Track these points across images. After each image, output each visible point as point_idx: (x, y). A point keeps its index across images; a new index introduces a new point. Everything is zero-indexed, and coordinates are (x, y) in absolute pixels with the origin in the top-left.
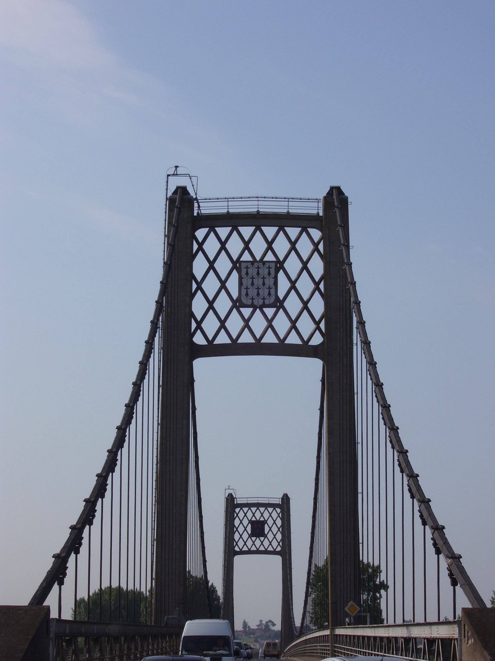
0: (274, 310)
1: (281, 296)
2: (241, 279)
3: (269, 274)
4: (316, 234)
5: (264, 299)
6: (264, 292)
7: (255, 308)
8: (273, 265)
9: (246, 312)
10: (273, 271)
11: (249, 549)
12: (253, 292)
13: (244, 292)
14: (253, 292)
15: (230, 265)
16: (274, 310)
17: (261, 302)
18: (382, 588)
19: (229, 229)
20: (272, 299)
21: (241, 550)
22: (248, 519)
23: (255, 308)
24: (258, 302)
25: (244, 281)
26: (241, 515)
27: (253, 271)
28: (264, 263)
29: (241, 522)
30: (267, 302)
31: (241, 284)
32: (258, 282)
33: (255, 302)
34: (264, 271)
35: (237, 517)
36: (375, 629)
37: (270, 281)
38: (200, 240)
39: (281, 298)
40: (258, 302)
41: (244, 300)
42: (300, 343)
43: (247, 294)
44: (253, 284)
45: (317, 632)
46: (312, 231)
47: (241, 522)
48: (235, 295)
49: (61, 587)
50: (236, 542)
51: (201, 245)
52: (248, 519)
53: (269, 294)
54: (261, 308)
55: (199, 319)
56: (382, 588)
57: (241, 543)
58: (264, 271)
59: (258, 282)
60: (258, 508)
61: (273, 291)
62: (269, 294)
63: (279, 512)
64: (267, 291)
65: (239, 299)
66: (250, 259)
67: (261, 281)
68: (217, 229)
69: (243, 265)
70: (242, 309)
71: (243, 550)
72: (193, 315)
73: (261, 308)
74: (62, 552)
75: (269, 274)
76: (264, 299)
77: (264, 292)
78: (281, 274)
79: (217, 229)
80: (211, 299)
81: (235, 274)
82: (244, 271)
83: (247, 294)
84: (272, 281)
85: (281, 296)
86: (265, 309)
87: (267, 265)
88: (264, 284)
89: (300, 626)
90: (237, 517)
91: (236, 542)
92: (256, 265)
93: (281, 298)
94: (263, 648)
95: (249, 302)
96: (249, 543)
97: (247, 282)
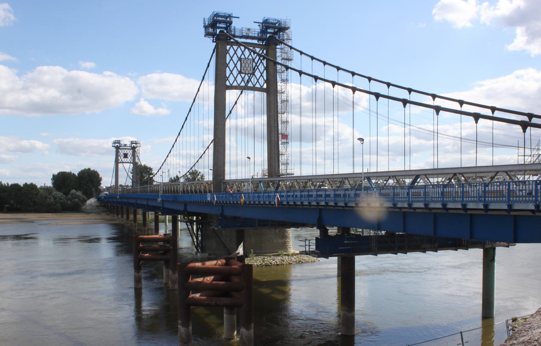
3: (251, 63)
5: (249, 71)
9: (243, 75)
10: (252, 62)
17: (248, 72)
18: (252, 250)
21: (231, 85)
22: (238, 57)
24: (247, 72)
25: (242, 65)
26: (232, 52)
28: (249, 59)
33: (246, 72)
34: (249, 62)
36: (45, 184)
40: (247, 72)
45: (192, 239)
49: (185, 208)
52: (238, 57)
56: (252, 250)
57: (231, 79)
58: (249, 62)
60: (239, 85)
64: (250, 69)
66: (244, 57)
67: (248, 65)
68: (233, 46)
69: (242, 59)
70: (241, 74)
71: (233, 85)
75: (251, 63)
76: (249, 71)
79: (233, 46)
80: (231, 70)
87: (250, 60)
88: (249, 66)
92: (246, 59)
94: (203, 260)
95: (244, 72)
96: (128, 152)
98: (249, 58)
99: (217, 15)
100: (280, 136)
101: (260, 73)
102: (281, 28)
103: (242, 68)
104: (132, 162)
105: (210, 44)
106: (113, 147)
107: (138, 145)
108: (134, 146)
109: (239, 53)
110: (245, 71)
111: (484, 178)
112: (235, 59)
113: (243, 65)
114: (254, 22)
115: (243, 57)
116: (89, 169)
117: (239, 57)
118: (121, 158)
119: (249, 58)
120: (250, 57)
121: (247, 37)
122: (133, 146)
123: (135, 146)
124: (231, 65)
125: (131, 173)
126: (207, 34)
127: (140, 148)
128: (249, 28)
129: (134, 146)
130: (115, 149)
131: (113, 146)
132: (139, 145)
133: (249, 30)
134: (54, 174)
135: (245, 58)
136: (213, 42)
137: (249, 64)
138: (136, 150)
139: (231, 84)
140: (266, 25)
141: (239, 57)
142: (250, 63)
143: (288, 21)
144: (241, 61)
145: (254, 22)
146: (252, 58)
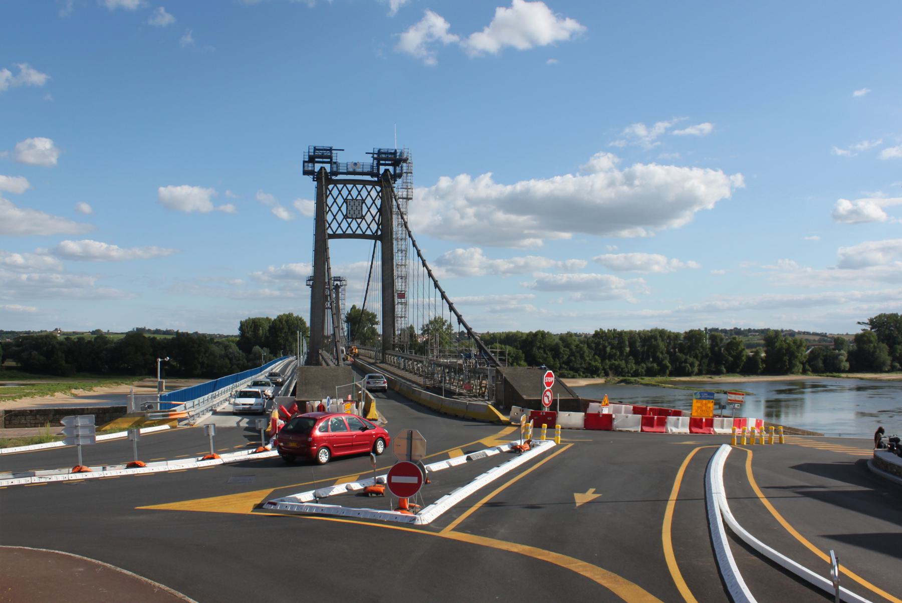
0: (361, 220)
1: (364, 214)
2: (347, 206)
3: (359, 205)
4: (378, 188)
5: (357, 215)
6: (357, 212)
7: (353, 219)
8: (361, 201)
9: (349, 220)
10: (360, 204)
11: (345, 185)
12: (352, 212)
13: (348, 212)
14: (352, 212)
15: (343, 201)
16: (361, 220)
17: (355, 217)
19: (362, 186)
20: (360, 216)
22: (343, 198)
23: (353, 219)
24: (354, 216)
25: (349, 208)
26: (335, 192)
27: (352, 203)
28: (357, 200)
29: (335, 201)
30: (358, 217)
31: (347, 209)
32: (354, 208)
34: (357, 203)
35: (330, 195)
37: (359, 208)
38: (330, 190)
39: (364, 215)
40: (354, 216)
41: (348, 215)
42: (372, 234)
43: (350, 213)
44: (352, 209)
46: (376, 187)
47: (335, 201)
48: (345, 214)
50: (328, 207)
51: (330, 192)
52: (343, 198)
53: (359, 213)
54: (355, 219)
55: (330, 223)
57: (334, 226)
59: (354, 208)
60: (364, 233)
61: (360, 212)
62: (359, 213)
63: (378, 191)
65: (346, 215)
68: (347, 185)
69: (348, 201)
70: (348, 219)
72: (327, 205)
73: (355, 219)
74: (501, 423)
75: (359, 205)
76: (357, 215)
77: (357, 212)
78: (364, 205)
79: (347, 185)
80: (335, 198)
81: (345, 204)
82: (348, 203)
83: (350, 213)
84: (360, 208)
85: (364, 214)
86: (357, 220)
87: (358, 201)
89: (255, 399)
90: (330, 212)
91: (328, 207)
93: (364, 215)
95: (351, 217)
96: (344, 225)
97: (350, 208)
98: (358, 198)
99: (315, 149)
100: (396, 295)
101: (342, 227)
102: (396, 159)
103: (348, 212)
104: (330, 187)
105: (310, 184)
106: (308, 286)
107: (344, 283)
108: (337, 284)
109: (345, 192)
110: (352, 215)
111: (131, 408)
112: (340, 201)
113: (350, 208)
114: (366, 153)
115: (350, 197)
116: (290, 315)
117: (345, 198)
118: (335, 221)
119: (358, 198)
120: (359, 198)
121: (354, 173)
122: (335, 284)
123: (339, 285)
124: (335, 209)
125: (346, 322)
126: (306, 173)
127: (346, 286)
128: (356, 162)
129: (337, 284)
130: (311, 289)
131: (307, 285)
132: (344, 284)
133: (355, 164)
134: (242, 320)
135: (353, 199)
136: (314, 180)
137: (357, 206)
138: (340, 290)
139: (344, 231)
140: (380, 156)
141: (345, 198)
142: (358, 204)
143: (405, 150)
144: (346, 203)
145: (366, 153)
146: (361, 199)
